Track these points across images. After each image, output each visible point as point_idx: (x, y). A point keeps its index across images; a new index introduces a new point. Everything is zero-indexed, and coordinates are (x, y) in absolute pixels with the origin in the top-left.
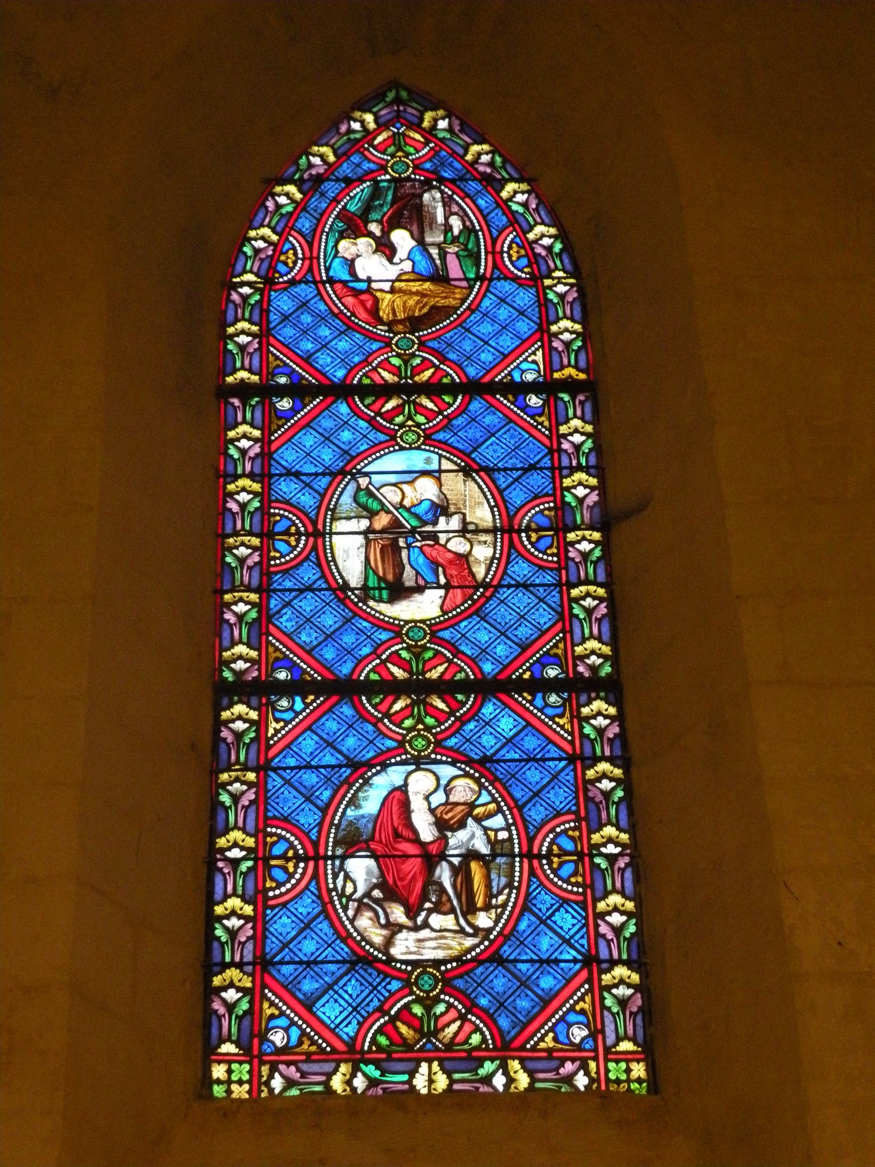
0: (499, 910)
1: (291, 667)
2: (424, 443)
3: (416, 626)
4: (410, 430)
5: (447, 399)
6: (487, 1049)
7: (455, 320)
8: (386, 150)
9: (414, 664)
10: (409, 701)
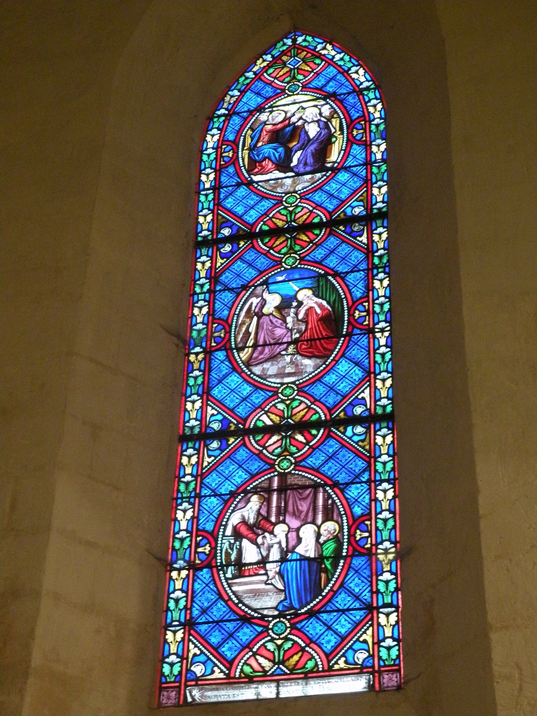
0: (335, 116)
1: (231, 226)
2: (301, 91)
3: (287, 387)
4: (291, 204)
5: (314, 432)
6: (318, 671)
7: (321, 600)
8: (280, 251)
9: (276, 654)
10: (279, 437)
